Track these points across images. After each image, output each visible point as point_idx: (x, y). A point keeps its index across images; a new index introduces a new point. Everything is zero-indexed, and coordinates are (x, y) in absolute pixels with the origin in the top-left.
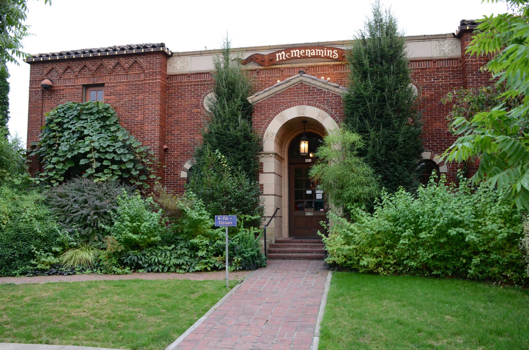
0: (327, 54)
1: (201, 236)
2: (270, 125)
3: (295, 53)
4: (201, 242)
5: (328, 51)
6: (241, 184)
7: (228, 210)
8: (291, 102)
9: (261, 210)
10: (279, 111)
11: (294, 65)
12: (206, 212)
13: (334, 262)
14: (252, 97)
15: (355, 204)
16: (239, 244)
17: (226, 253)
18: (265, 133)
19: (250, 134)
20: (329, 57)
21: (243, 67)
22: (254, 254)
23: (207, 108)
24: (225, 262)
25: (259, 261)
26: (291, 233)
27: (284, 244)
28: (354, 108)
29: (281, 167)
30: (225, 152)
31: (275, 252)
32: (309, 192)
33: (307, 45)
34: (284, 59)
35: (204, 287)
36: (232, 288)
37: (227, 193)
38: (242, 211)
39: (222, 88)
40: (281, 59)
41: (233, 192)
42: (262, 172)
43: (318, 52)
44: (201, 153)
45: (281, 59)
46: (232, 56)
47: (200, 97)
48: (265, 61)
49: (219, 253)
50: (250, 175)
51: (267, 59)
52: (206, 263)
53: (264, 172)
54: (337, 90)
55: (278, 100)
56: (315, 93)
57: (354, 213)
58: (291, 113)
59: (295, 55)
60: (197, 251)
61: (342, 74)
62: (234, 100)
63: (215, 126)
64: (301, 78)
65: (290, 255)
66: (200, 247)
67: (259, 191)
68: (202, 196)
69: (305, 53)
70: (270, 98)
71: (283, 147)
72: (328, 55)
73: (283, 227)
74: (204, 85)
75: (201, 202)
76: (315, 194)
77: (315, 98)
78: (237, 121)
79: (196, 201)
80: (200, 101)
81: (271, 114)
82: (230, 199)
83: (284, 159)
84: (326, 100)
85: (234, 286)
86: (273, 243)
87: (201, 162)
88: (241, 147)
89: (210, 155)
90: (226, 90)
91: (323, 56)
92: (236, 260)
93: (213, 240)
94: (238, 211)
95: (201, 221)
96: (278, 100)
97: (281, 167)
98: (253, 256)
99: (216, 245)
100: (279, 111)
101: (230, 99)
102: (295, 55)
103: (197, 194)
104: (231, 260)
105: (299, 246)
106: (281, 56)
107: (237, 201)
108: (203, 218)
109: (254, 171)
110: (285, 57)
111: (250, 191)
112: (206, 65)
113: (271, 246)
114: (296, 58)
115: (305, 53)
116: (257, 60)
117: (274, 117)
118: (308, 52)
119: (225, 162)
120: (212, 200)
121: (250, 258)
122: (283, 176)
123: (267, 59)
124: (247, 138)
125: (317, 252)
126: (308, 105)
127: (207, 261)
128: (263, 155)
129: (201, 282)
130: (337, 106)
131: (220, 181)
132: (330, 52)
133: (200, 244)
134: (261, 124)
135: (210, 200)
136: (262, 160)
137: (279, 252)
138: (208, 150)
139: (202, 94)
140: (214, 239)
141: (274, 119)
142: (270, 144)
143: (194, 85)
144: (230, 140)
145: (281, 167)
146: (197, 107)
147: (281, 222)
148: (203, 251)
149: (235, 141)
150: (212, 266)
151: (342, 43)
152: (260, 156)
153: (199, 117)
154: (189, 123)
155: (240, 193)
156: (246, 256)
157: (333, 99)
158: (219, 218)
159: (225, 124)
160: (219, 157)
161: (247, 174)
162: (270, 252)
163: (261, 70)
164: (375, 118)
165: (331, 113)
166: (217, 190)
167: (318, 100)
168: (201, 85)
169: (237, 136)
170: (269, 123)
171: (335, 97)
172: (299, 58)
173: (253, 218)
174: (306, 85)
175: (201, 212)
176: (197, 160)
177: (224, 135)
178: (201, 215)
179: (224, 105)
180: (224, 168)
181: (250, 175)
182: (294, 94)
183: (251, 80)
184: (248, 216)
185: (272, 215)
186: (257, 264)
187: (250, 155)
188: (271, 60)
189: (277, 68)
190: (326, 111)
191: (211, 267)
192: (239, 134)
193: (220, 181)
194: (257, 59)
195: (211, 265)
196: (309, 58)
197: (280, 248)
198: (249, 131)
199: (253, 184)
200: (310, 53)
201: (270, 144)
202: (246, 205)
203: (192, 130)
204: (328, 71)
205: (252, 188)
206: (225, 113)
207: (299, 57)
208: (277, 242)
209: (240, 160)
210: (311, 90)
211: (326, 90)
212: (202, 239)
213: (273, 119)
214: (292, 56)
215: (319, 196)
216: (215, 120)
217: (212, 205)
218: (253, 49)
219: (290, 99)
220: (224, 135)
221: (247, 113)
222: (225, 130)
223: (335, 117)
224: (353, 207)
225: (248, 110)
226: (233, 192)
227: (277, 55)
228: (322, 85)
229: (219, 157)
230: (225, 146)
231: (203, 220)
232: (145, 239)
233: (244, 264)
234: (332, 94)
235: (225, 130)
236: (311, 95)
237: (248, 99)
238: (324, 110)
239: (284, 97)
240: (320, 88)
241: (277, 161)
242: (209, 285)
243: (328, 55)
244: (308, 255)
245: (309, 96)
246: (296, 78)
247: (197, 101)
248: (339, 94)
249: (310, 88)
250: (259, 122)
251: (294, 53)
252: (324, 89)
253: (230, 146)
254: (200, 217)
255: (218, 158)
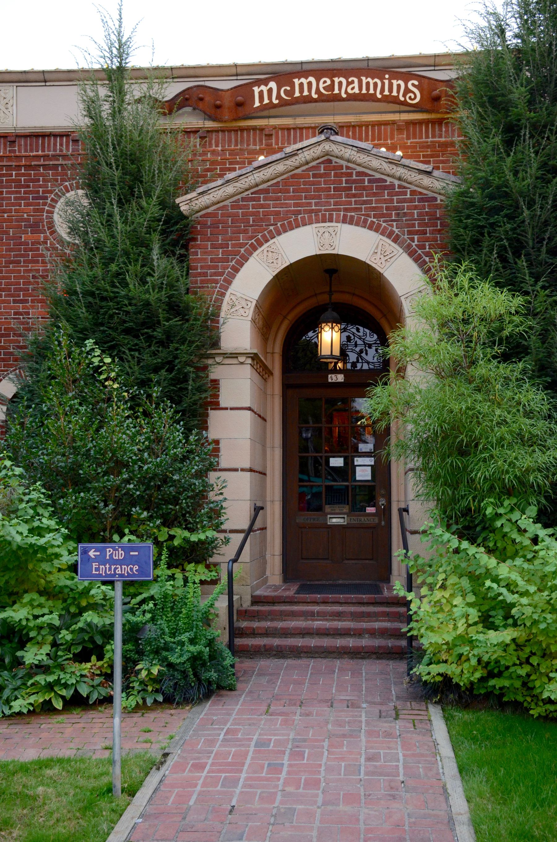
0: (391, 90)
1: (35, 596)
2: (239, 275)
3: (303, 85)
4: (36, 617)
5: (395, 82)
6: (159, 440)
7: (122, 514)
8: (299, 212)
9: (216, 513)
10: (264, 236)
11: (300, 121)
12: (52, 523)
13: (447, 679)
14: (189, 196)
15: (506, 503)
16: (153, 619)
17: (116, 649)
18: (227, 299)
19: (185, 298)
20: (395, 101)
21: (165, 123)
22: (200, 653)
23: (62, 230)
24: (109, 677)
25: (213, 675)
26: (289, 572)
27: (277, 608)
28: (483, 227)
29: (263, 394)
30: (112, 348)
31: (253, 633)
32: (337, 462)
33: (335, 66)
34: (275, 102)
35: (35, 798)
36: (131, 792)
37: (120, 465)
38: (162, 516)
39: (105, 168)
40: (266, 101)
41: (135, 463)
42: (216, 406)
43: (368, 84)
44: (42, 351)
45: (266, 101)
46: (135, 91)
47: (42, 200)
48: (224, 104)
49: (90, 648)
50: (184, 412)
51: (227, 102)
52: (50, 687)
53: (222, 405)
54: (426, 181)
55: (262, 206)
56: (364, 188)
57: (506, 529)
58: (299, 244)
59: (306, 93)
60: (22, 645)
61: (428, 147)
62: (139, 204)
63: (85, 273)
64: (327, 146)
65: (299, 642)
66: (32, 634)
67: (208, 456)
68: (43, 474)
69: (331, 88)
70: (242, 201)
71: (270, 342)
72: (395, 93)
73: (268, 557)
74: (55, 167)
75: (37, 493)
76: (354, 467)
77: (365, 202)
78: (147, 262)
79: (21, 490)
80: (42, 210)
81: (242, 245)
82: (128, 481)
83: (271, 373)
84: (396, 208)
85: (141, 783)
86: (247, 604)
87: (42, 375)
88: (158, 333)
89: (69, 354)
90: (117, 174)
91: (379, 96)
92: (144, 673)
93: (73, 609)
94: (150, 518)
95: (36, 552)
96: (262, 206)
97: (265, 393)
98: (195, 659)
99: (80, 625)
100: (264, 236)
101: (128, 201)
102: (306, 93)
103: (28, 467)
104: (128, 672)
105: (321, 615)
106: (267, 93)
107: (148, 488)
108: (42, 541)
109: (195, 403)
110: (279, 96)
111: (184, 458)
112: (62, 112)
113: (244, 614)
114: (308, 100)
115: (331, 88)
116: (201, 104)
117: (251, 254)
118: (340, 83)
119: (113, 375)
120: (75, 484)
121: (188, 665)
122: (268, 419)
123: (227, 102)
124: (176, 308)
125: (372, 633)
126: (344, 221)
127: (51, 679)
128: (218, 359)
129: (24, 768)
130: (427, 225)
131: (97, 430)
132: (399, 86)
133: (31, 624)
134: (216, 274)
135: (64, 486)
136: (216, 373)
137: (267, 633)
138: (64, 341)
139: (51, 192)
140: (78, 606)
141: (251, 260)
142: (238, 330)
143: (28, 167)
144: (127, 313)
145: (265, 393)
146: (35, 227)
147: (263, 541)
148: (40, 644)
149: (142, 316)
150: (67, 693)
151: (432, 62)
152: (210, 361)
153: (42, 255)
154: (12, 271)
155: (158, 466)
156: (173, 659)
157: (416, 207)
158: (92, 553)
159: (113, 267)
160: (96, 361)
161: (176, 412)
162: (243, 633)
163: (210, 131)
164: (543, 256)
165: (409, 246)
166: (87, 455)
167: (373, 209)
168: (45, 167)
169: (147, 304)
170: (237, 271)
171: (420, 200)
172: (315, 101)
173: (194, 538)
174: (341, 167)
175: (36, 524)
176: (32, 370)
177: (112, 299)
178: (38, 531)
179: (110, 215)
180: (111, 393)
181: (184, 412)
182: (307, 190)
183: (186, 153)
184: (180, 534)
185: (245, 525)
186: (210, 683)
187: (185, 358)
188: (240, 105)
189: (254, 128)
190: (395, 241)
191: (63, 697)
192: (153, 297)
193: (97, 430)
194: (201, 99)
195: (64, 692)
196: (343, 100)
197: (266, 620)
198: (183, 290)
199: (192, 438)
200: (345, 86)
201: (238, 330)
202: (176, 501)
203: (21, 289)
204: (392, 139)
205: (190, 452)
206: (113, 236)
207: (315, 96)
208: (256, 600)
209: (156, 370)
210: (355, 181)
211: (397, 183)
212: (40, 606)
213: (247, 260)
214: (297, 94)
215: (363, 473)
216: (85, 258)
217: (70, 500)
218: (191, 72)
219: (296, 205)
220: (112, 299)
221: (175, 244)
222: (114, 286)
223: (420, 257)
224: (501, 511)
225: (179, 233)
226: (135, 463)
227: (256, 90)
228: (386, 167)
229: (96, 361)
230: (115, 329)
231: (43, 549)
232: (522, 214)
233: (167, 686)
234: (413, 193)
235: (114, 286)
236: (354, 196)
237: (177, 201)
238: (389, 237)
239: (278, 199)
240: (378, 176)
241: (256, 377)
242: (53, 781)
243: (395, 93)
244: (351, 642)
245: (347, 196)
246: (310, 149)
247: (35, 210)
248: (431, 194)
249: (351, 174)
250: (209, 267)
251: (301, 85)
252: (389, 179)
253: (127, 331)
254: (33, 540)
255: (92, 363)
